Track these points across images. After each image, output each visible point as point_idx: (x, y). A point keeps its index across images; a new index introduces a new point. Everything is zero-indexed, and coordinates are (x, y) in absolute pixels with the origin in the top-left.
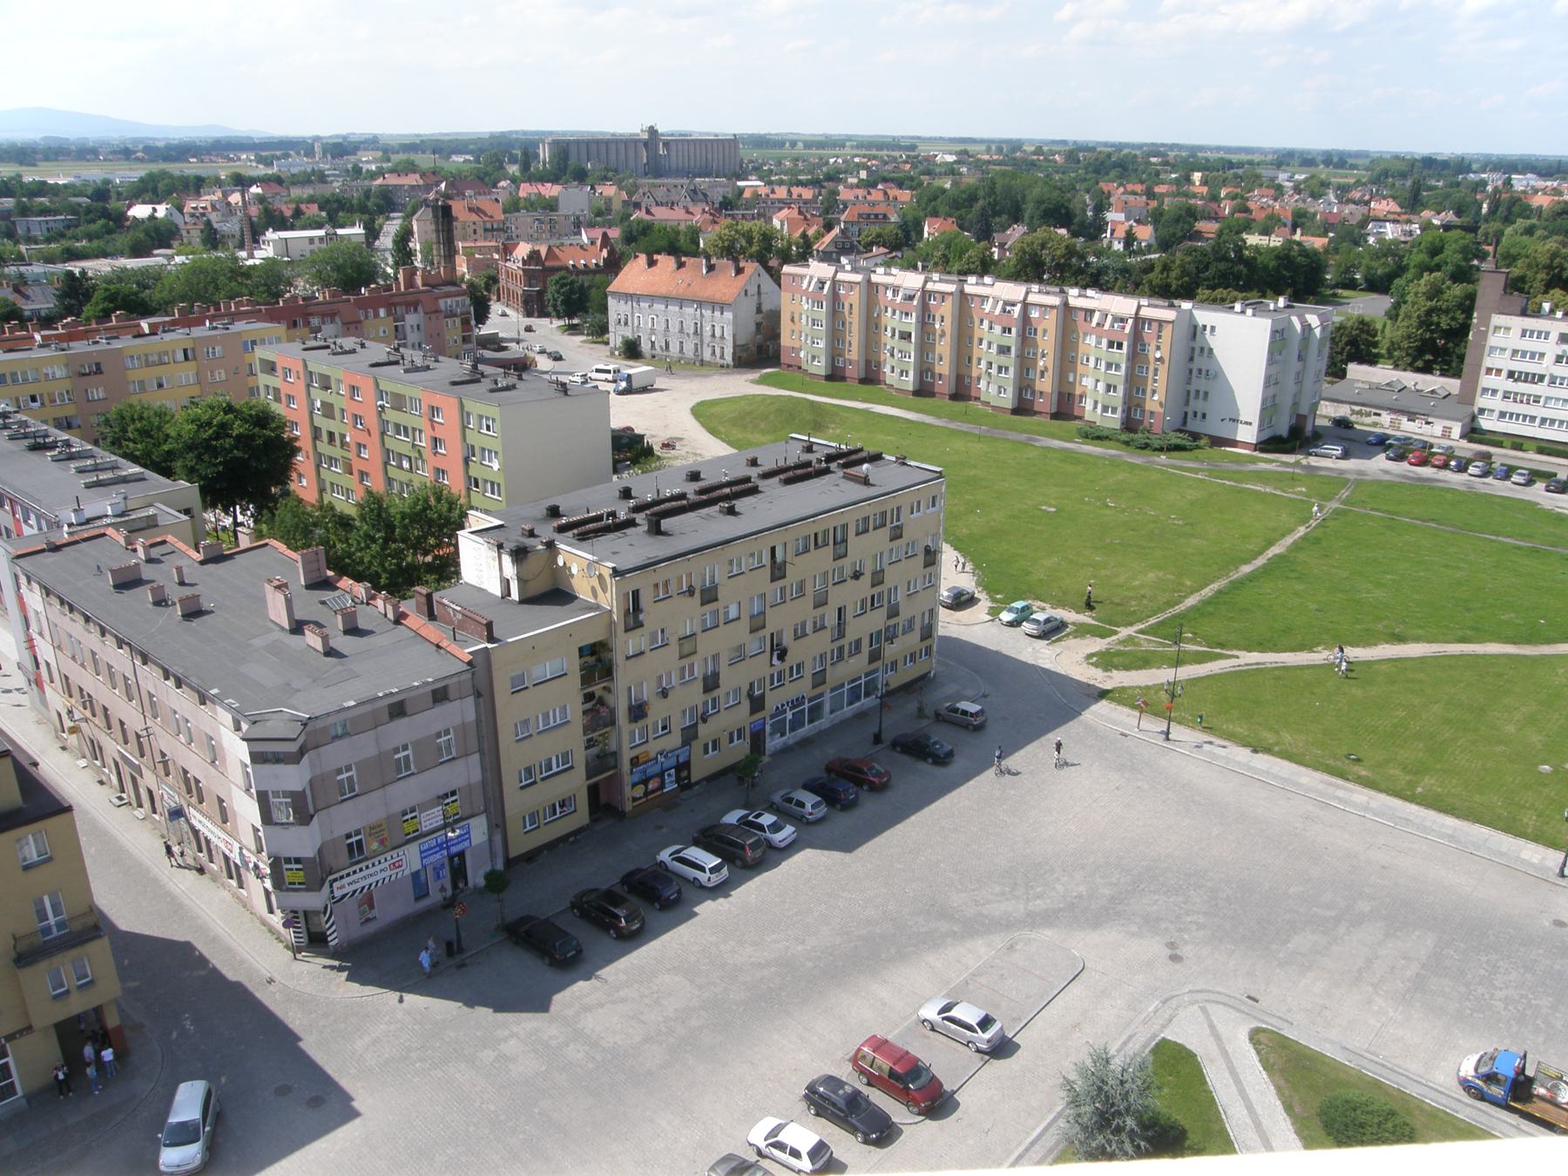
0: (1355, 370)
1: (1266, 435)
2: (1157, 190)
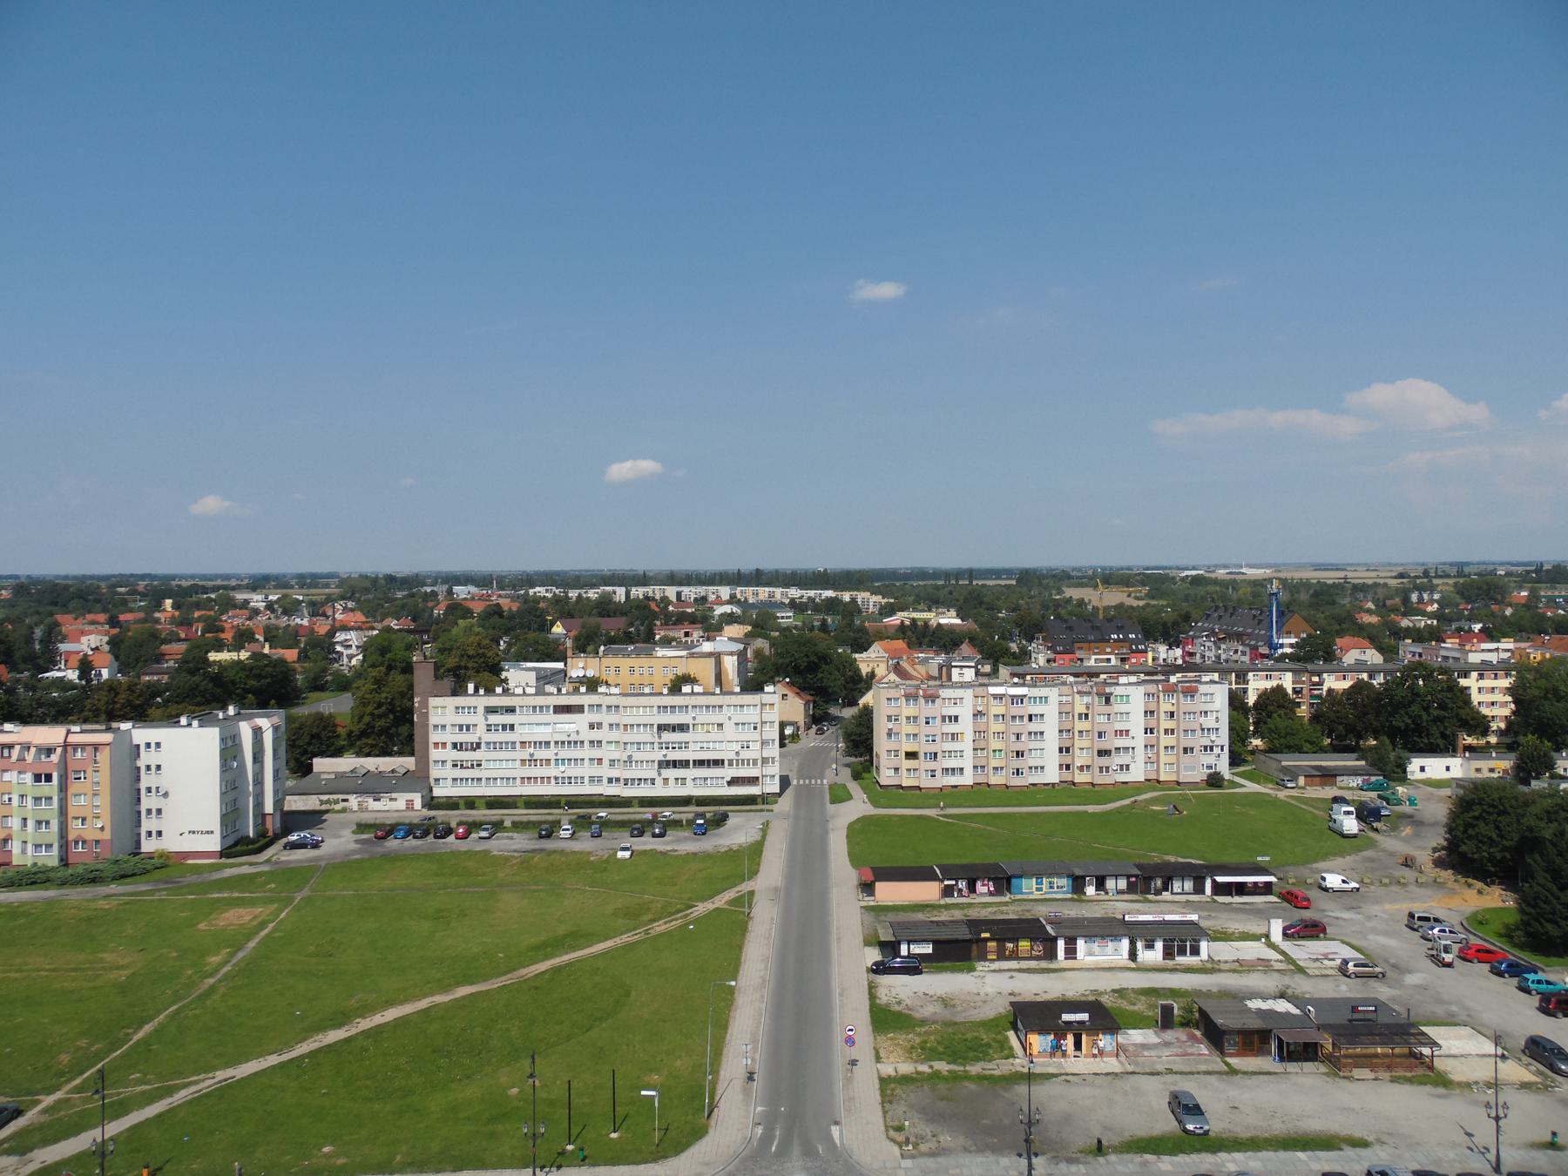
0: (320, 764)
1: (230, 841)
2: (122, 617)
